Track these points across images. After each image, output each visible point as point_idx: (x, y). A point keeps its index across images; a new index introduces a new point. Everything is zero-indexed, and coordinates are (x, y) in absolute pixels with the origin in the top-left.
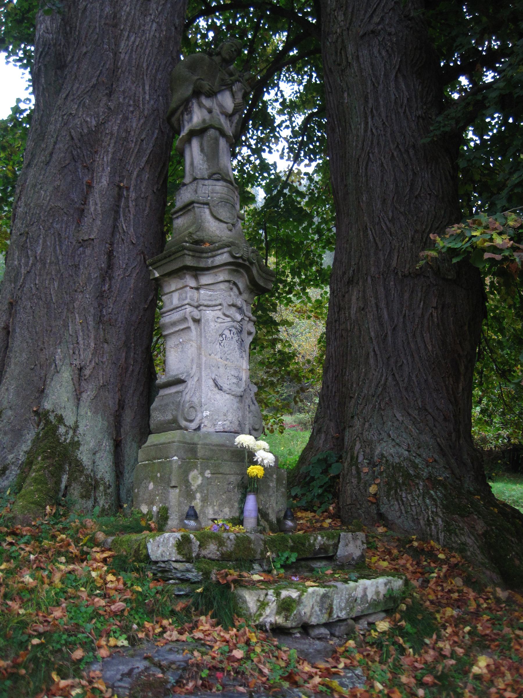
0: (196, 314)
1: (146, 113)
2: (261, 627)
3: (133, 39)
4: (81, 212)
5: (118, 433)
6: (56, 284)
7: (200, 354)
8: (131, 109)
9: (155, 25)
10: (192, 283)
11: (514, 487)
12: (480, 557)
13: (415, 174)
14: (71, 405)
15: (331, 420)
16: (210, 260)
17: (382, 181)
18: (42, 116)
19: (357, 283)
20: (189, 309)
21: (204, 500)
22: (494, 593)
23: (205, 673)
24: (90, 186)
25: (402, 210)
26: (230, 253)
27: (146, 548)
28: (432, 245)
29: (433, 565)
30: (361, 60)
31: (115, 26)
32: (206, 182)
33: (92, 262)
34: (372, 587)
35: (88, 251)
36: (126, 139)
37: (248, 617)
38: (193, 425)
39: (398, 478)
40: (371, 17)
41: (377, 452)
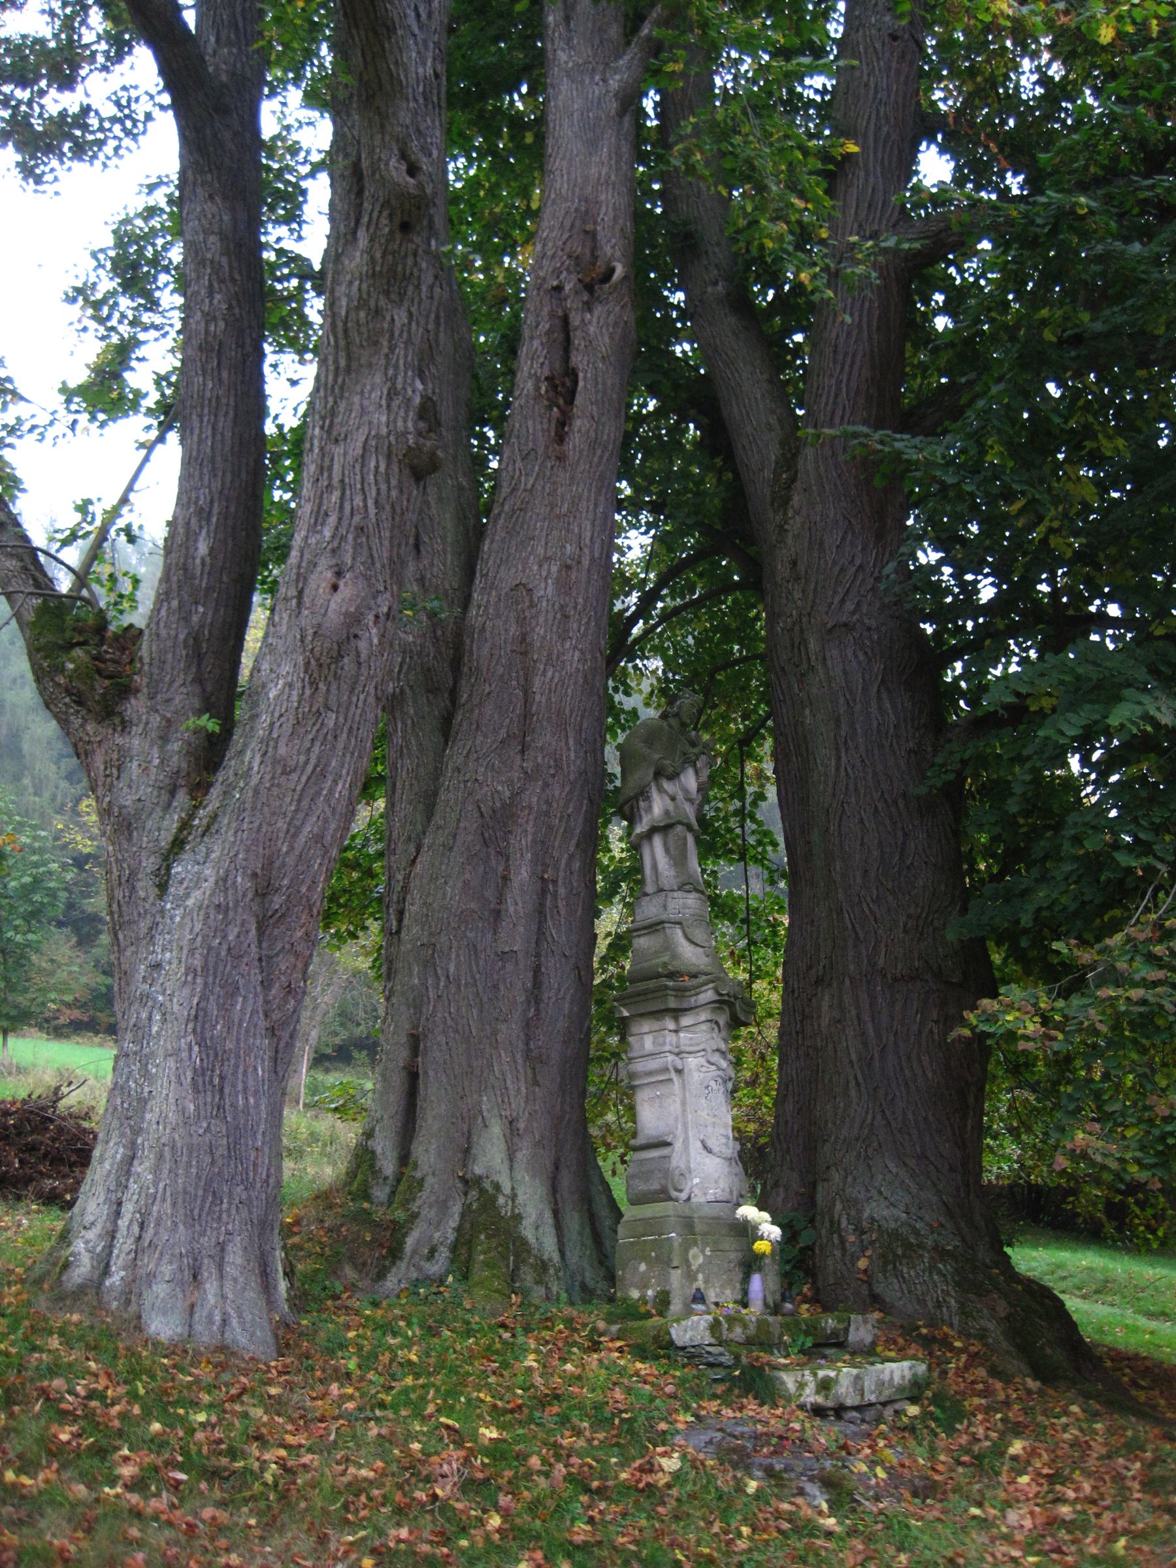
1: (572, 777)
2: (802, 1407)
3: (550, 674)
4: (497, 914)
5: (556, 1203)
6: (475, 1011)
7: (684, 1111)
8: (552, 771)
9: (577, 653)
10: (671, 1025)
11: (1034, 1254)
12: (1005, 1345)
13: (905, 834)
14: (504, 1168)
15: (792, 1169)
16: (693, 999)
17: (862, 844)
18: (418, 765)
19: (830, 984)
20: (671, 1058)
21: (706, 1281)
22: (1024, 1384)
23: (774, 1441)
24: (506, 879)
25: (890, 886)
26: (716, 990)
27: (669, 1334)
28: (964, 1022)
29: (949, 1355)
30: (829, 663)
31: (525, 653)
32: (675, 894)
33: (518, 980)
34: (898, 1371)
35: (509, 967)
36: (547, 814)
37: (788, 1399)
38: (684, 1196)
39: (896, 1249)
40: (843, 601)
41: (866, 1215)
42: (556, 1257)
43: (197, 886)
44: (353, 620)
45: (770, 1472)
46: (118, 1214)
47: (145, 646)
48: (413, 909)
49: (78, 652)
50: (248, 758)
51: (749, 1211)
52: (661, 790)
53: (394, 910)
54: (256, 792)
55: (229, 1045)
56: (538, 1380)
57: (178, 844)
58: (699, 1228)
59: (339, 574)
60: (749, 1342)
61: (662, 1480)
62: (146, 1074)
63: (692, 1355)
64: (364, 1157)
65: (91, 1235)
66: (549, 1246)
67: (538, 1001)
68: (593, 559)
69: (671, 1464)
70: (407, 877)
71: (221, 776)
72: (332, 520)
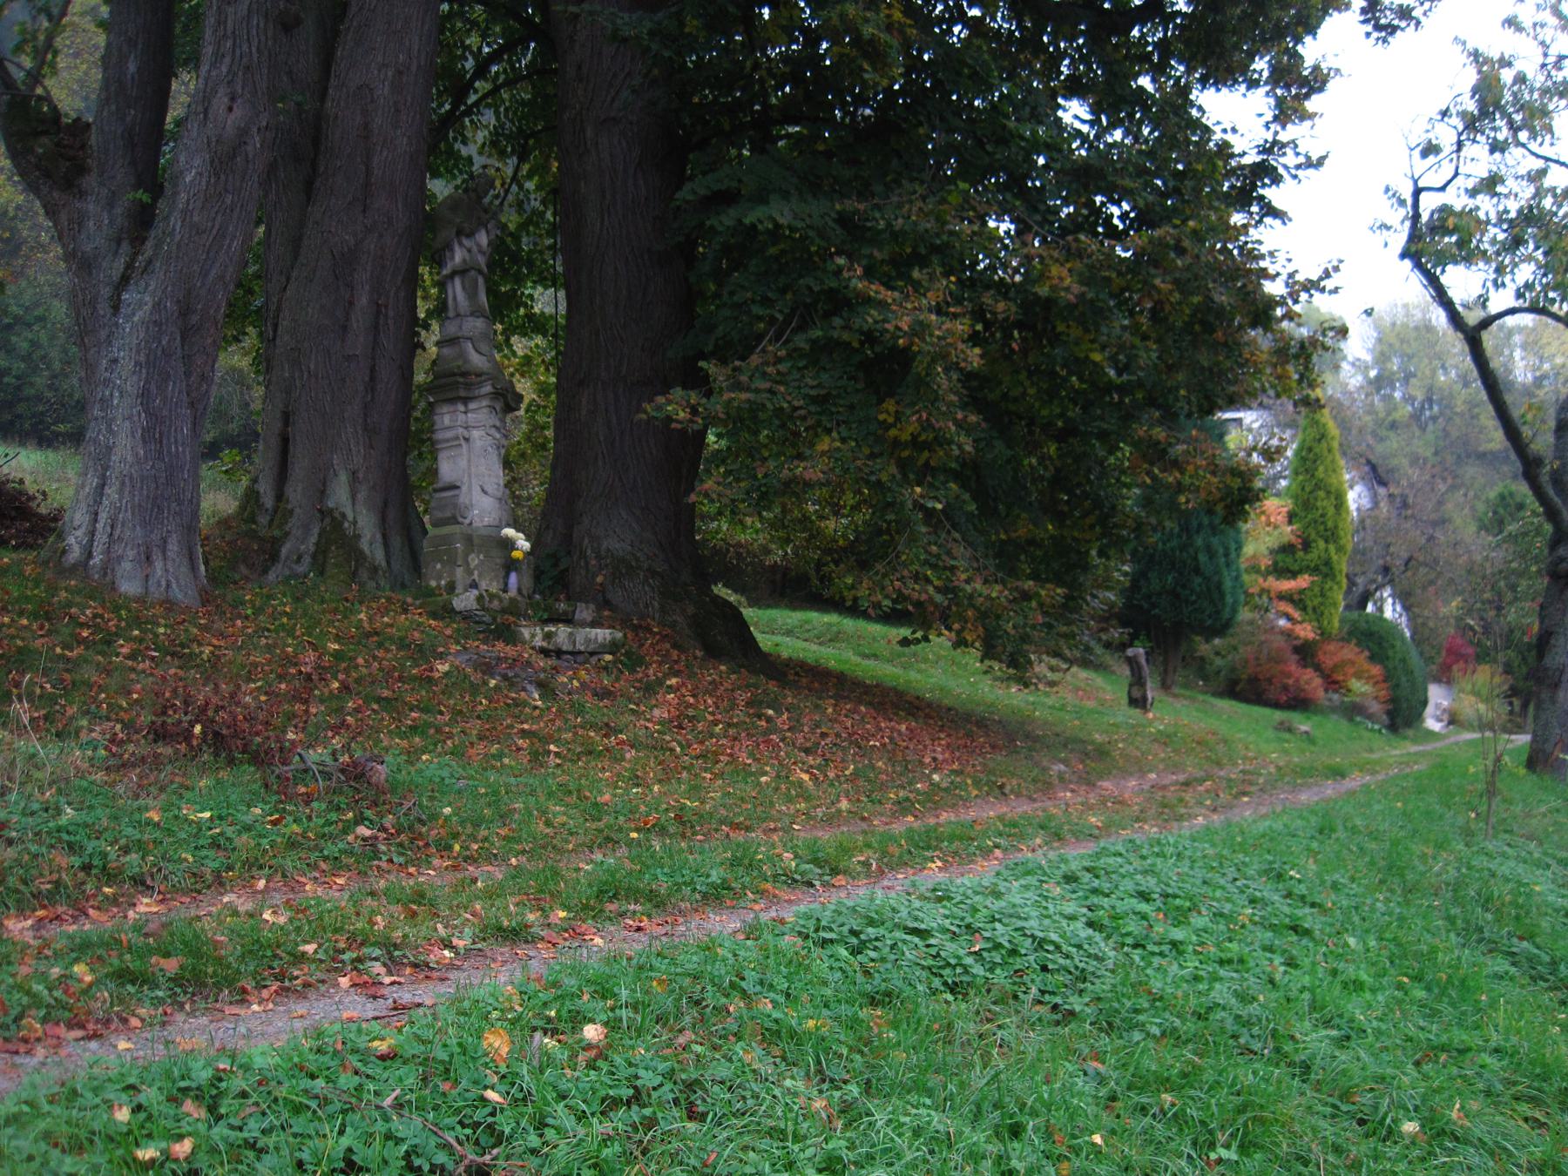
0: (466, 434)
2: (533, 648)
4: (345, 328)
10: (462, 408)
24: (351, 303)
34: (602, 634)
37: (524, 642)
42: (384, 564)
43: (140, 308)
44: (243, 133)
45: (505, 678)
46: (96, 521)
47: (93, 137)
48: (284, 323)
49: (45, 140)
50: (172, 221)
51: (509, 532)
52: (461, 244)
53: (267, 320)
54: (179, 246)
55: (165, 413)
56: (366, 625)
57: (124, 281)
58: (476, 541)
59: (233, 99)
60: (504, 611)
61: (437, 675)
62: (110, 431)
63: (466, 616)
64: (251, 497)
65: (79, 533)
66: (379, 556)
67: (373, 390)
68: (419, 67)
69: (443, 668)
70: (280, 301)
71: (153, 233)
72: (227, 60)
